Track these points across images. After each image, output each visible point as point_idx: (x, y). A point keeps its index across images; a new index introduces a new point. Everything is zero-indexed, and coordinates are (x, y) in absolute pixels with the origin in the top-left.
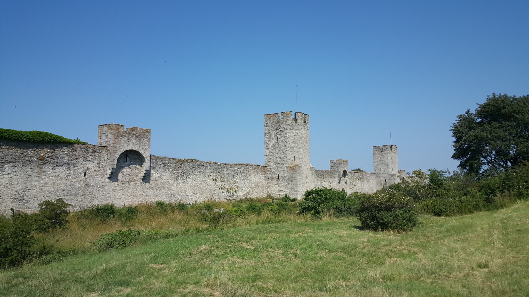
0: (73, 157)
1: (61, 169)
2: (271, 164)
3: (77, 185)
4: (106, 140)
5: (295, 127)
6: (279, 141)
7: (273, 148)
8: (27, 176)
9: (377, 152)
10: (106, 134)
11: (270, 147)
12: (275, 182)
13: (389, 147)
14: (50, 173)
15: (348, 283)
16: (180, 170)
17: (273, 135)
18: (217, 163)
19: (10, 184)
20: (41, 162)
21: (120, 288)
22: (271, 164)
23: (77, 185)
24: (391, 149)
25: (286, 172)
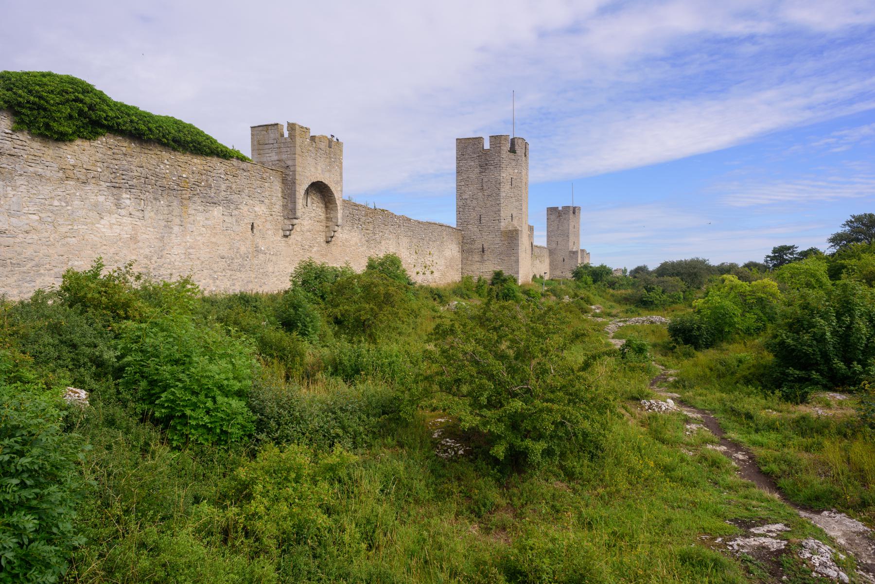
0: (234, 186)
1: (217, 212)
2: (469, 226)
3: (243, 249)
4: (275, 158)
5: (514, 163)
6: (485, 187)
7: (473, 197)
8: (163, 223)
9: (553, 217)
10: (276, 145)
11: (467, 197)
12: (477, 258)
13: (571, 209)
14: (200, 218)
15: (259, 488)
16: (371, 227)
17: (473, 176)
18: (410, 220)
19: (134, 239)
20: (180, 192)
21: (657, 442)
22: (469, 226)
23: (243, 249)
24: (574, 213)
25: (497, 240)
